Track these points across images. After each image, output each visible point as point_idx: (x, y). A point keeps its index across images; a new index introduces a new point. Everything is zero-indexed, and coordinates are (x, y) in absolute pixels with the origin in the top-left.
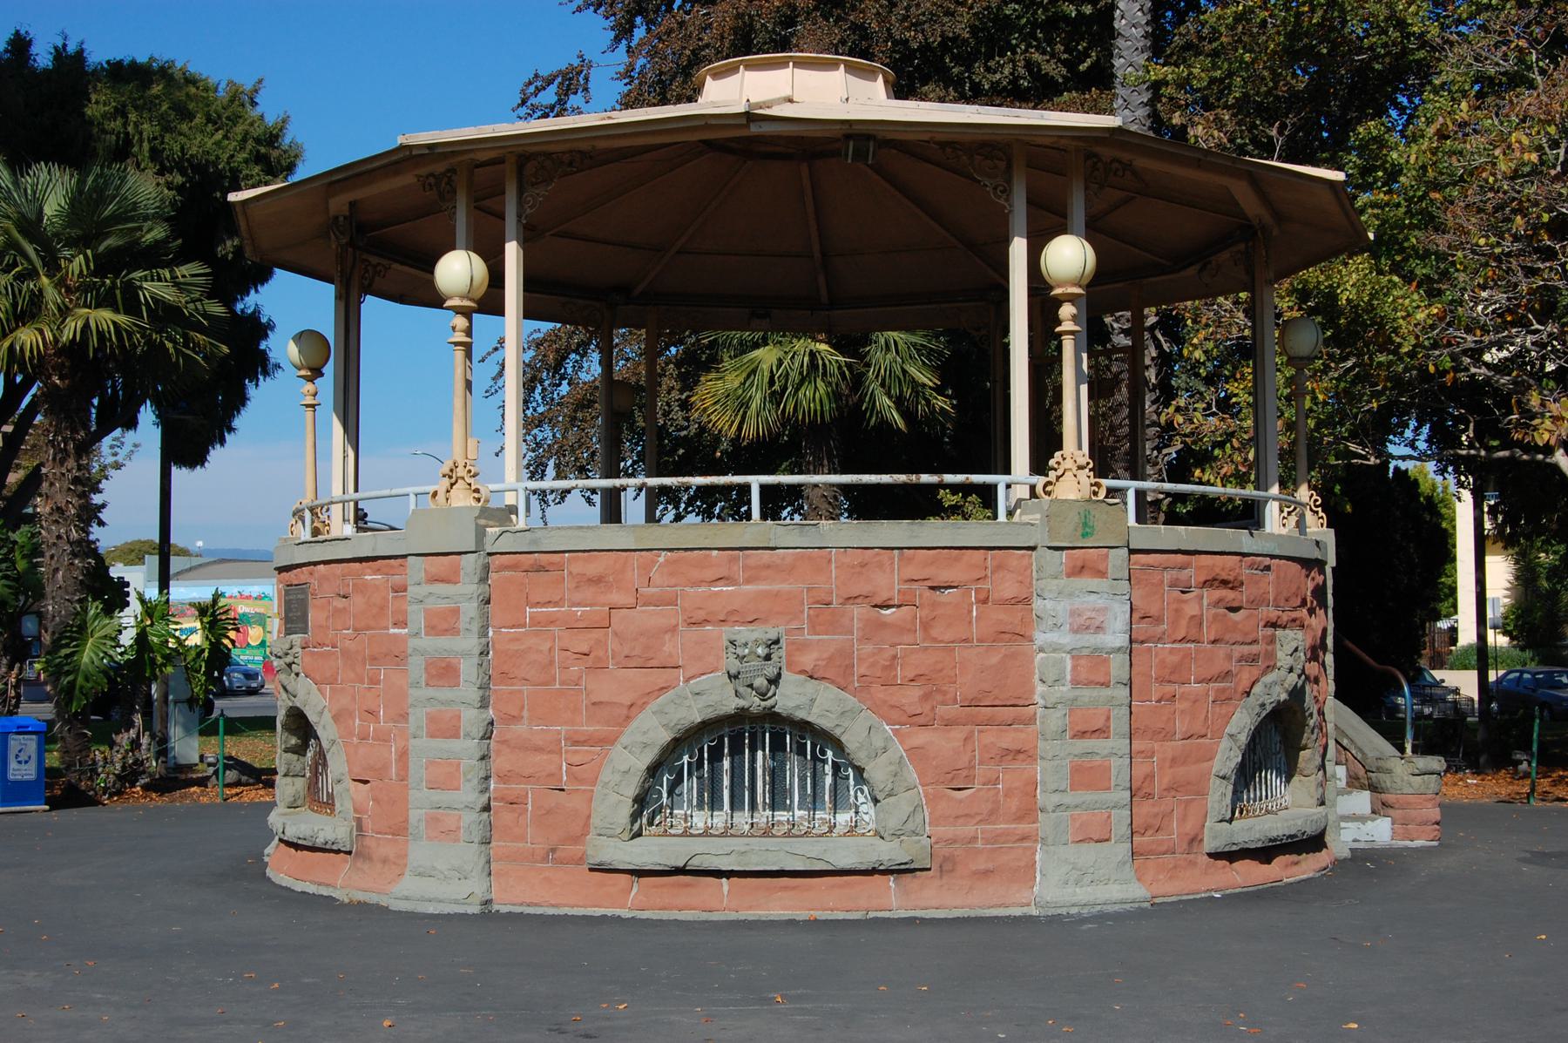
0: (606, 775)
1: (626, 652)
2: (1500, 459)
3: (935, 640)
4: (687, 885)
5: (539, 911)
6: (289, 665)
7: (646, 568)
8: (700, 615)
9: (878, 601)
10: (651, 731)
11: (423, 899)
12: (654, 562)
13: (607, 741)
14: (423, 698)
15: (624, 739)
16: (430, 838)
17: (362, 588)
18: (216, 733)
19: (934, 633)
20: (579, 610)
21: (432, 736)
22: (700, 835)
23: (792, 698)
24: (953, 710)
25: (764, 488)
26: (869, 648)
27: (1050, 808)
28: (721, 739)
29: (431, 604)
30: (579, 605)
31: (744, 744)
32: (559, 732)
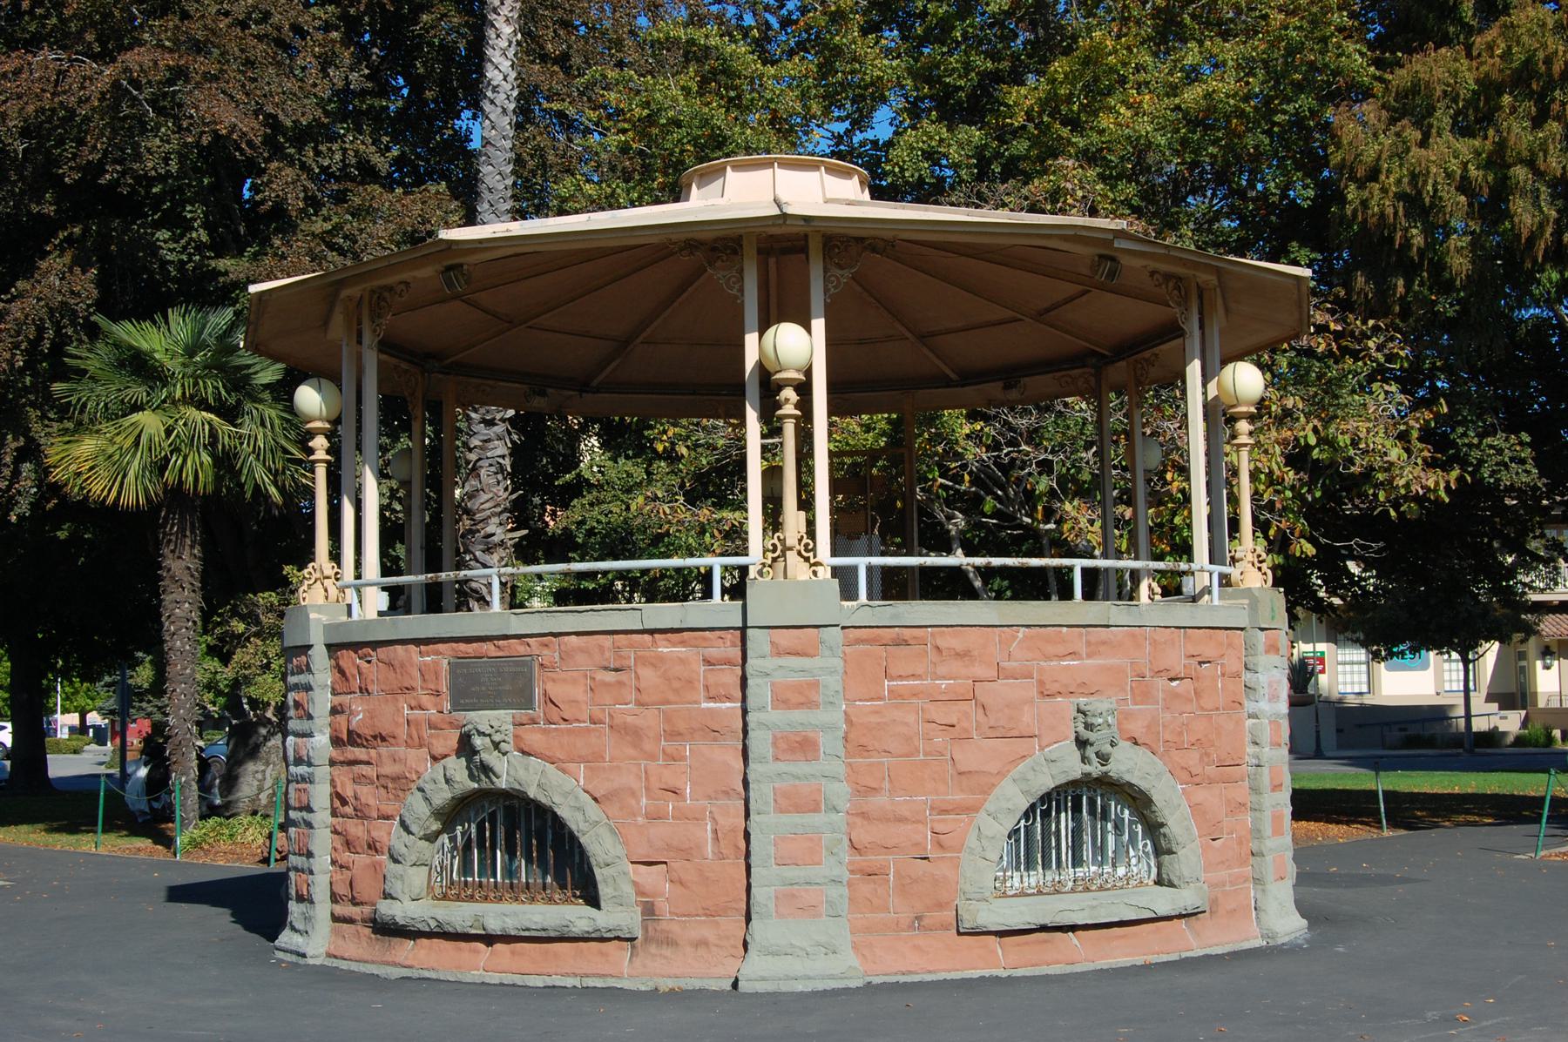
3: (1202, 709)
4: (1045, 941)
5: (916, 978)
8: (1054, 688)
9: (1172, 675)
11: (788, 978)
16: (780, 915)
17: (657, 662)
18: (1553, 799)
20: (944, 684)
21: (781, 810)
22: (1015, 896)
23: (1128, 764)
24: (1211, 770)
26: (1168, 716)
28: (493, 819)
29: (778, 677)
30: (944, 678)
31: (1087, 805)
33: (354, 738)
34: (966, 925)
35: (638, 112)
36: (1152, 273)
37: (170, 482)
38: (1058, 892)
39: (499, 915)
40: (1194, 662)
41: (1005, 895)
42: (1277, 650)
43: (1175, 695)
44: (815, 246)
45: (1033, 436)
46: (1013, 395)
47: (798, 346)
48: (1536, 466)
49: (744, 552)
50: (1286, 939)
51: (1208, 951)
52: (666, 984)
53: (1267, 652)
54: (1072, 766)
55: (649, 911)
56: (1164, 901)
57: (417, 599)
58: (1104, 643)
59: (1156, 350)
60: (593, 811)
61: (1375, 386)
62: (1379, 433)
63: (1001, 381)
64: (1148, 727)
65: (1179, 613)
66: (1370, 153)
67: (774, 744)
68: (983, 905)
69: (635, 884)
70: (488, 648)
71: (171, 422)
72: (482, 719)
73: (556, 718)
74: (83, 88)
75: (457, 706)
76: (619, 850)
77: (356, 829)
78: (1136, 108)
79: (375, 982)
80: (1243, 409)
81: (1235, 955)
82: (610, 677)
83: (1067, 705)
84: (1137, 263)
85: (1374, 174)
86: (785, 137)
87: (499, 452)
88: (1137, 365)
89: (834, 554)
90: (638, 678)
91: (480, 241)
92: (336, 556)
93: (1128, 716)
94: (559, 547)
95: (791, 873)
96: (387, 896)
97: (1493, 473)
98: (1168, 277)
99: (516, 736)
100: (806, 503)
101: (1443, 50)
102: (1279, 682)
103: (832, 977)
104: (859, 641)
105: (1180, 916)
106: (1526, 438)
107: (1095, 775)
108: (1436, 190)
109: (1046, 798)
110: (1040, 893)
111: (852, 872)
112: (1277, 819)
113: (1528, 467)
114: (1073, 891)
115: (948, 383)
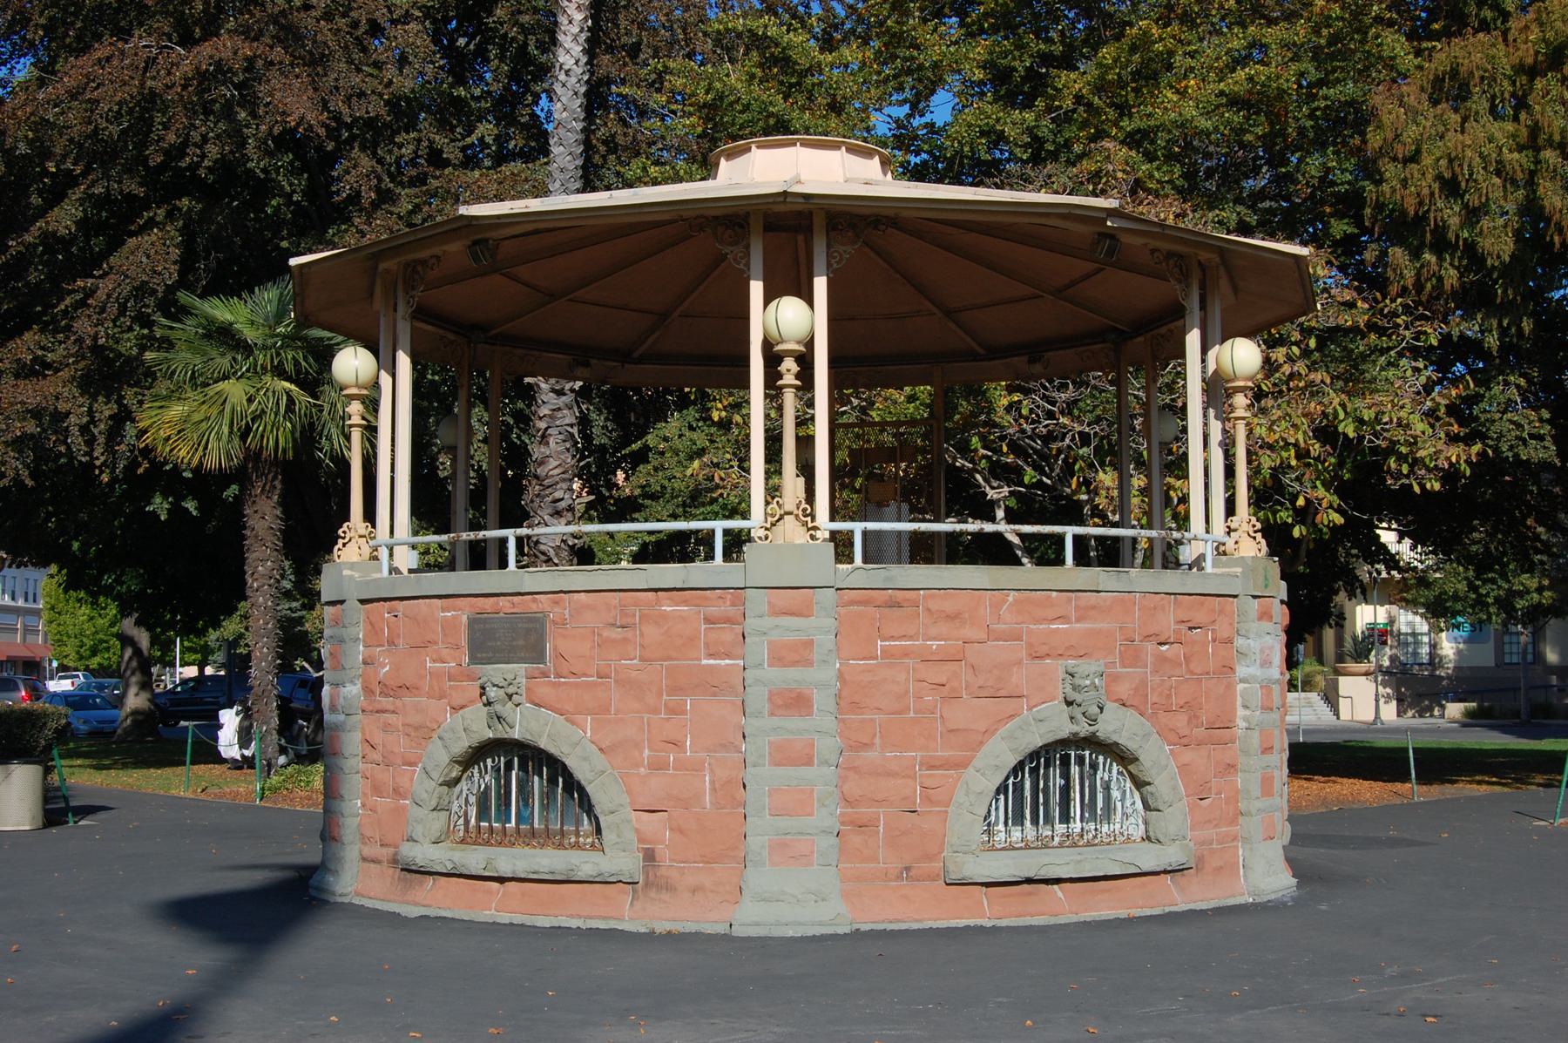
0: (960, 796)
1: (981, 683)
2: (1418, 537)
3: (1192, 673)
4: (1030, 894)
5: (904, 926)
6: (510, 697)
7: (995, 607)
8: (1044, 650)
10: (1001, 753)
11: (778, 924)
12: (1005, 601)
13: (962, 764)
14: (765, 728)
15: (977, 763)
19: (1192, 666)
23: (1116, 725)
24: (1199, 732)
25: (865, 533)
26: (1157, 679)
27: (1254, 811)
29: (775, 636)
30: (934, 639)
32: (914, 758)
33: (386, 689)
34: (954, 876)
35: (702, 97)
36: (1153, 251)
37: (253, 447)
38: (1046, 847)
39: (509, 860)
40: (1183, 627)
41: (993, 849)
42: (1270, 618)
43: (1162, 660)
44: (819, 222)
45: (1070, 408)
46: (1037, 368)
47: (792, 319)
48: (1555, 443)
49: (745, 515)
50: (1273, 897)
51: (1192, 906)
52: (661, 927)
53: (1260, 618)
54: (1060, 725)
55: (650, 856)
56: (1149, 858)
57: (462, 556)
58: (1093, 608)
59: (1171, 326)
60: (600, 761)
61: (1403, 362)
62: (1404, 409)
63: (1031, 358)
64: (1136, 689)
65: (1170, 580)
66: (1412, 132)
67: (770, 699)
68: (971, 858)
69: (637, 830)
70: (502, 601)
71: (252, 391)
72: (496, 672)
73: (565, 673)
74: (169, 73)
75: (474, 660)
76: (626, 799)
77: (384, 776)
78: (1182, 93)
79: (394, 920)
80: (1241, 384)
81: (1219, 911)
82: (616, 634)
83: (1059, 667)
84: (1139, 241)
85: (1414, 158)
86: (833, 118)
87: (567, 421)
88: (1149, 342)
89: (832, 519)
90: (642, 635)
91: (499, 217)
92: (370, 515)
93: (1115, 678)
94: (627, 509)
95: (785, 823)
96: (411, 839)
97: (1511, 448)
98: (1170, 255)
99: (528, 689)
100: (806, 469)
101: (1481, 35)
102: (1271, 648)
103: (820, 924)
104: (853, 603)
105: (1166, 872)
106: (1546, 415)
107: (1082, 735)
108: (1471, 175)
109: (1034, 755)
110: (1027, 847)
111: (843, 823)
112: (1267, 783)
113: (1547, 444)
114: (1061, 845)
115: (976, 357)
